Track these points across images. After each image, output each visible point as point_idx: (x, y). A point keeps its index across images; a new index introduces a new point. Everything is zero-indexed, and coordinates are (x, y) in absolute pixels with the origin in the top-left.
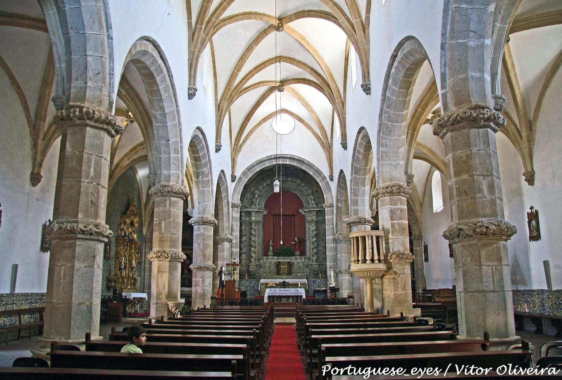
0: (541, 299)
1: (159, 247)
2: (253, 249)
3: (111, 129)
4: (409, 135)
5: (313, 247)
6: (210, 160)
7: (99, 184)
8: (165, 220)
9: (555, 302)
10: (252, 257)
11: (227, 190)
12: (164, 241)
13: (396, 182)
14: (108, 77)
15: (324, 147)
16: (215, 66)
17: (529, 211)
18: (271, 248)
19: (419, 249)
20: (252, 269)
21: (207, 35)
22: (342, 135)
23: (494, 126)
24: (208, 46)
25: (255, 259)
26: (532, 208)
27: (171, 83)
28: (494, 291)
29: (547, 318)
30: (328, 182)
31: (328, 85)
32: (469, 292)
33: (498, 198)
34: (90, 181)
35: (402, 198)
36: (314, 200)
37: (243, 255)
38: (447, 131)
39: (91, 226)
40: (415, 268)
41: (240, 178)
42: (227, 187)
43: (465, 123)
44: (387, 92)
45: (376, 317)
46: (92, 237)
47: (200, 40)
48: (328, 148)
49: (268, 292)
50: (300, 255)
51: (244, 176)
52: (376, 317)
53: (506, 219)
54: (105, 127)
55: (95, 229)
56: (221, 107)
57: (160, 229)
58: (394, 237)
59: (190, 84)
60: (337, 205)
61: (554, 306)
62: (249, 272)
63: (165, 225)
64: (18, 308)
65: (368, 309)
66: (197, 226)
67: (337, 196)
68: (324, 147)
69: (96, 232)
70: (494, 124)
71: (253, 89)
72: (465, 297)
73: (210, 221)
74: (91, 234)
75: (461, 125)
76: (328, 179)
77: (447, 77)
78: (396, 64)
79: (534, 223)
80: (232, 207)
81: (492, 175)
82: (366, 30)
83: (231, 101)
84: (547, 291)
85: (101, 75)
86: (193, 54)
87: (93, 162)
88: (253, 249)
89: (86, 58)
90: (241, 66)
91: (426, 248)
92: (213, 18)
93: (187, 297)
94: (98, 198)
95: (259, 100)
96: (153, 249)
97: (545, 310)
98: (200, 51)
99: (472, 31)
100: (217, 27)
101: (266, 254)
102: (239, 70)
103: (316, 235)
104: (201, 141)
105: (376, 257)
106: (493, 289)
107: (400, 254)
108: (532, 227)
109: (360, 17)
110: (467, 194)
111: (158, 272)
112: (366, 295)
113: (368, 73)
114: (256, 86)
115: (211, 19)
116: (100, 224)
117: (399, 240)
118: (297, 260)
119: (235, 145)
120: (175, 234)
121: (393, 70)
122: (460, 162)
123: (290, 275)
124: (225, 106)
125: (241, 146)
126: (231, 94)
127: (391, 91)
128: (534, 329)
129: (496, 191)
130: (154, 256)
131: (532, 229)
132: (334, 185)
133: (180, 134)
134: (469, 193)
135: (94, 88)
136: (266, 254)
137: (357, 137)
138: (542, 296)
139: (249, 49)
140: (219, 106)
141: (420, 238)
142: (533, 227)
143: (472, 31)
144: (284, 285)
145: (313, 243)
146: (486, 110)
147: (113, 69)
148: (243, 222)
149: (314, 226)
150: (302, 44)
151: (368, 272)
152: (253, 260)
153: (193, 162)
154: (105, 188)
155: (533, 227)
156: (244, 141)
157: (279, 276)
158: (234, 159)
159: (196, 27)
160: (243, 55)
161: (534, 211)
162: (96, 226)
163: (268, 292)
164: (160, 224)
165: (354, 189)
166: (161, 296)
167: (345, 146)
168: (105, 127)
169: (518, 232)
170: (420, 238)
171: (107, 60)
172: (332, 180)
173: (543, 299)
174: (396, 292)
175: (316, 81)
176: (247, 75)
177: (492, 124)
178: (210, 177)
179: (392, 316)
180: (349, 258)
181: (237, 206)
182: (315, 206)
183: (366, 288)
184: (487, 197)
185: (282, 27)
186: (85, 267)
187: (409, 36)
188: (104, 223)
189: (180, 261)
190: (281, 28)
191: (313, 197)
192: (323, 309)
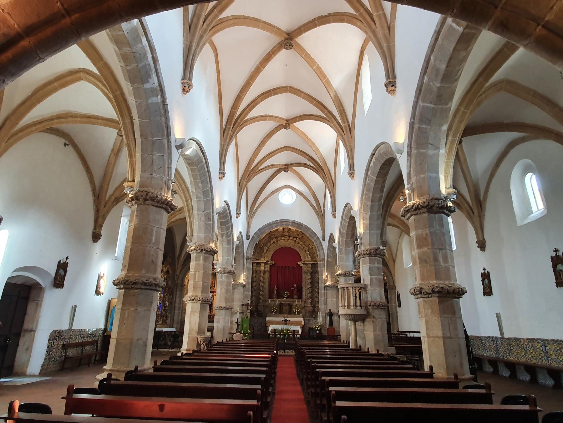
0: (496, 345)
1: (193, 292)
2: (261, 292)
3: (168, 207)
4: (384, 211)
5: (308, 292)
6: (232, 225)
7: (158, 248)
8: (198, 271)
9: (507, 348)
10: (261, 299)
11: (243, 247)
12: (197, 287)
13: (374, 247)
14: (167, 169)
15: (318, 215)
16: (238, 153)
17: (483, 272)
18: (275, 292)
19: (393, 297)
20: (260, 308)
21: (234, 133)
22: (332, 207)
23: (447, 212)
24: (234, 142)
25: (263, 301)
26: (484, 269)
27: (208, 169)
28: (450, 338)
29: (502, 361)
30: (320, 241)
31: (322, 169)
32: (430, 337)
33: (452, 266)
34: (152, 246)
35: (379, 258)
36: (310, 255)
37: (253, 297)
38: (412, 215)
39: (151, 280)
40: (390, 312)
41: (253, 237)
42: (243, 244)
43: (425, 210)
44: (367, 179)
45: (359, 352)
46: (151, 287)
47: (229, 136)
48: (321, 214)
49: (271, 328)
50: (298, 299)
51: (256, 235)
52: (359, 352)
53: (458, 282)
54: (164, 206)
55: (154, 282)
56: (241, 184)
57: (195, 278)
58: (373, 289)
59: (220, 169)
60: (327, 260)
61: (507, 351)
62: (257, 311)
63: (198, 275)
64: (73, 342)
65: (352, 346)
66: (220, 275)
67: (328, 253)
68: (318, 214)
69: (155, 284)
70: (447, 211)
71: (265, 170)
72: (428, 341)
73: (230, 271)
74: (151, 285)
75: (422, 211)
76: (321, 239)
77: (412, 175)
78: (374, 159)
79: (486, 281)
80: (246, 260)
81: (445, 248)
82: (352, 132)
83: (249, 179)
84: (500, 338)
85: (162, 169)
86: (223, 147)
87: (155, 232)
88: (261, 292)
89: (153, 157)
90: (258, 154)
91: (399, 296)
92: (239, 120)
93: (211, 330)
94: (157, 258)
95: (269, 178)
96: (188, 294)
97: (499, 354)
98: (228, 145)
99: (430, 144)
100: (242, 126)
101: (271, 296)
102: (256, 157)
103: (310, 283)
104: (226, 210)
105: (358, 304)
106: (449, 336)
107: (377, 302)
108: (485, 285)
109: (348, 122)
110: (426, 262)
111: (191, 312)
112: (351, 334)
113: (353, 164)
114: (268, 168)
115: (237, 121)
116: (157, 277)
117: (377, 291)
118: (295, 302)
119: (250, 211)
120: (206, 282)
121: (372, 164)
122: (421, 238)
123: (290, 314)
124: (244, 184)
125: (255, 213)
126: (249, 174)
127: (370, 179)
128: (491, 370)
129: (450, 261)
130: (189, 299)
131: (485, 286)
132: (325, 244)
133: (212, 207)
134: (428, 261)
135: (157, 178)
136: (271, 296)
137: (344, 210)
138: (497, 342)
139: (263, 142)
140: (240, 183)
141: (393, 288)
142: (486, 284)
143: (430, 144)
144: (286, 322)
145: (308, 289)
146: (441, 201)
147: (171, 164)
148: (254, 271)
149: (310, 276)
150: (303, 136)
151: (353, 316)
152: (261, 301)
153: (219, 225)
154: (162, 251)
155: (486, 284)
156: (257, 209)
157: (281, 315)
158: (249, 223)
159: (226, 127)
160: (259, 145)
161: (486, 272)
162: (155, 279)
163: (271, 328)
164: (195, 274)
165: (341, 249)
166: (192, 332)
167: (334, 215)
168: (164, 206)
169: (467, 292)
170: (394, 287)
171: (167, 158)
172: (324, 240)
173: (497, 345)
174: (375, 333)
175: (312, 165)
176: (261, 160)
177: (445, 211)
178: (231, 237)
179: (371, 352)
180: (338, 302)
181: (250, 259)
182: (310, 259)
183: (351, 329)
184: (442, 265)
185: (289, 126)
186: (144, 310)
187: (383, 142)
188: (160, 277)
189: (208, 304)
190: (288, 127)
191: (309, 253)
192: (316, 344)
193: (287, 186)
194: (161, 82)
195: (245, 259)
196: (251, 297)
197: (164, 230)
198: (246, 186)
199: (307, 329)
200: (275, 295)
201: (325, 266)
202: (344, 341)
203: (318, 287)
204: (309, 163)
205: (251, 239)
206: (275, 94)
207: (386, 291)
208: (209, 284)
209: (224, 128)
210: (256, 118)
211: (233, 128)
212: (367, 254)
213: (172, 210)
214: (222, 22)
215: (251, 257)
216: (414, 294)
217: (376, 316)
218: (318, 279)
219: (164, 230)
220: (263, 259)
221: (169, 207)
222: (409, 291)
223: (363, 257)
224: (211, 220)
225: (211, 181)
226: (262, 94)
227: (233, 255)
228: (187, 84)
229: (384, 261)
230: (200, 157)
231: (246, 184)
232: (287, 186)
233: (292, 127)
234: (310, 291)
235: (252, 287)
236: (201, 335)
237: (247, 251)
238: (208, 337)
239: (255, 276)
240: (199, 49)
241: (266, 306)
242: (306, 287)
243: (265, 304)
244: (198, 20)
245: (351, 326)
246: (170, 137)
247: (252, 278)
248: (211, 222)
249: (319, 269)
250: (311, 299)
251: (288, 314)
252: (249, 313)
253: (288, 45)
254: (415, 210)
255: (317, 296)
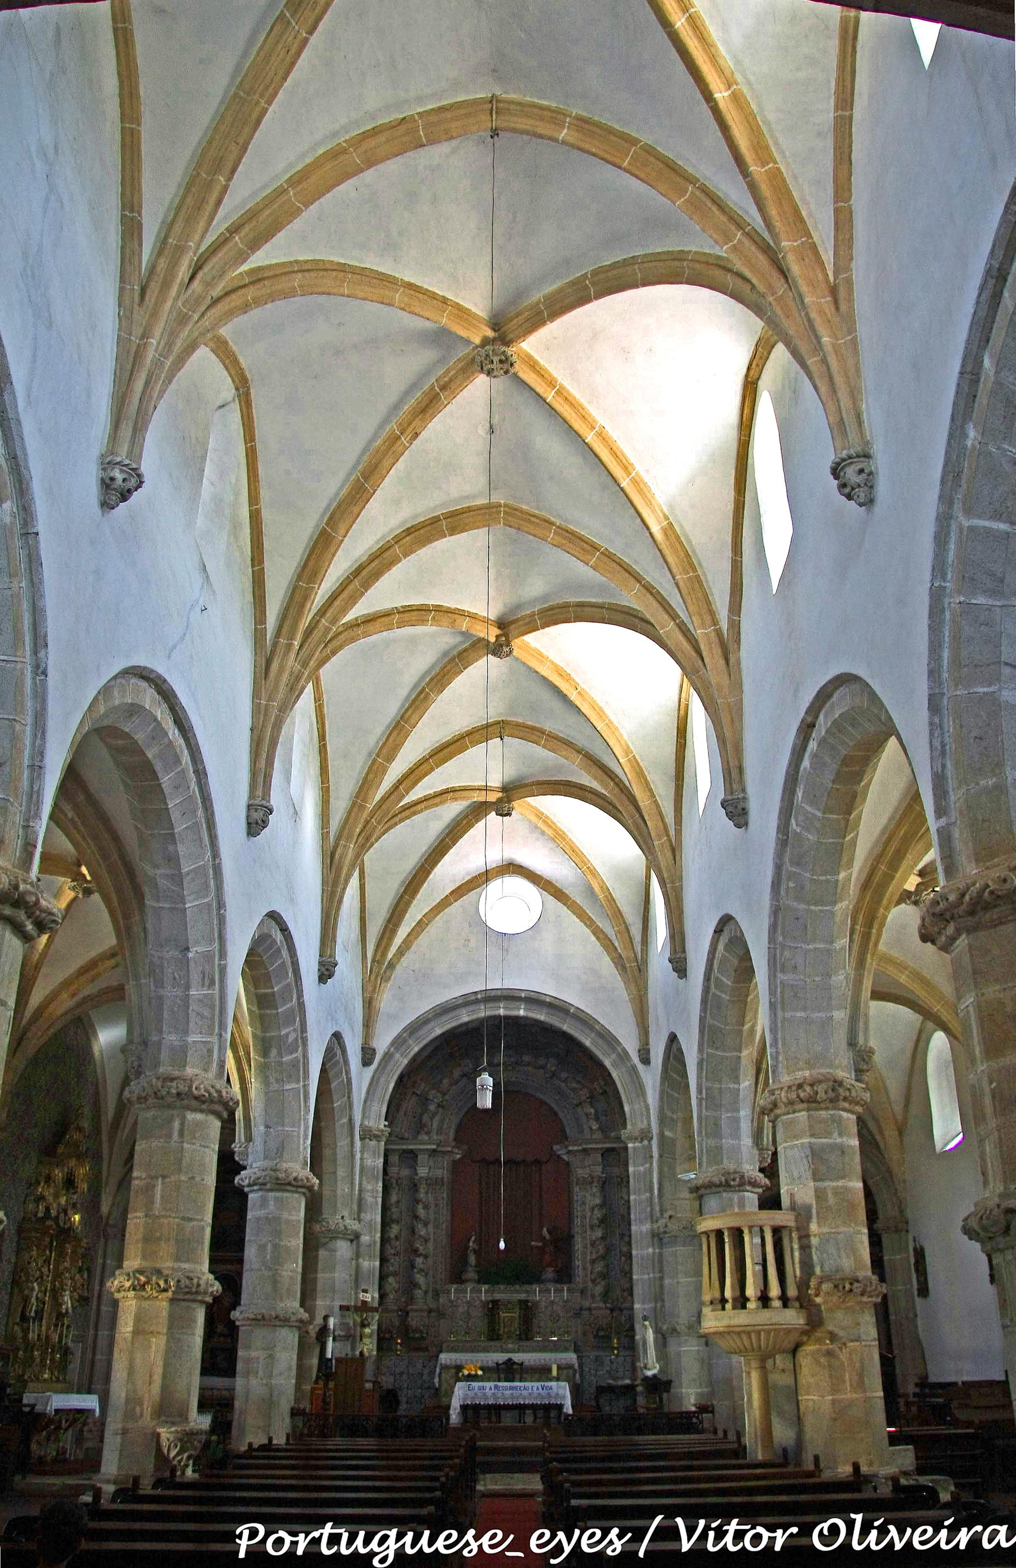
2: (419, 1261)
4: (856, 937)
8: (164, 1177)
10: (416, 1285)
12: (159, 1239)
16: (325, 745)
21: (305, 664)
25: (426, 1293)
30: (634, 1068)
36: (597, 1119)
37: (391, 1280)
38: (958, 932)
49: (460, 1394)
50: (557, 1281)
52: (782, 1476)
56: (337, 857)
59: (252, 795)
60: (661, 1135)
62: (405, 1330)
63: (163, 1191)
66: (260, 1193)
73: (295, 1179)
76: (636, 1059)
77: (951, 784)
78: (812, 745)
80: (361, 1139)
88: (419, 1261)
91: (920, 1255)
95: (443, 840)
98: (287, 706)
100: (332, 646)
101: (457, 1277)
102: (391, 758)
103: (602, 1221)
105: (774, 1291)
113: (741, 769)
119: (373, 961)
121: (806, 763)
124: (350, 854)
125: (391, 966)
126: (367, 822)
127: (801, 818)
130: (127, 1284)
132: (651, 1078)
144: (509, 1371)
149: (598, 1194)
153: (255, 1009)
159: (275, 644)
160: (402, 717)
163: (460, 1394)
170: (902, 1225)
172: (646, 1061)
175: (595, 785)
176: (411, 771)
178: (299, 1053)
179: (827, 1475)
182: (598, 1135)
183: (750, 1384)
189: (202, 1302)
190: (506, 649)
191: (592, 1111)
193: (512, 868)
194: (19, 453)
195: (357, 1137)
196: (382, 1278)
197: (213, 1150)
198: (358, 860)
199: (590, 1391)
200: (470, 1269)
201: (651, 1157)
202: (725, 1432)
203: (630, 1236)
204: (586, 779)
205: (379, 1065)
206: (453, 531)
207: (875, 1241)
208: (203, 1229)
209: (269, 649)
210: (387, 614)
211: (301, 647)
212: (802, 1101)
213: (41, 927)
214: (259, 280)
215: (382, 1131)
216: (982, 1234)
217: (841, 1333)
218: (629, 1208)
219: (213, 1150)
220: (426, 1138)
221: (29, 917)
222: (962, 1223)
223: (788, 1113)
224: (212, 983)
225: (216, 836)
226: (409, 531)
227: (306, 1120)
228: (122, 471)
229: (864, 1131)
230: (170, 742)
231: (358, 855)
232: (512, 868)
233: (520, 647)
234: (602, 1251)
235: (384, 1240)
236: (173, 1424)
237: (364, 1109)
238: (200, 1432)
239: (398, 1202)
240: (171, 359)
241: (438, 1311)
242: (584, 1238)
243: (433, 1306)
244: (174, 264)
245: (749, 1373)
246: (42, 654)
247: (385, 1208)
248: (217, 991)
249: (631, 1169)
250: (603, 1283)
251: (520, 1339)
252: (370, 1336)
253: (496, 359)
254: (972, 913)
255: (627, 1268)
